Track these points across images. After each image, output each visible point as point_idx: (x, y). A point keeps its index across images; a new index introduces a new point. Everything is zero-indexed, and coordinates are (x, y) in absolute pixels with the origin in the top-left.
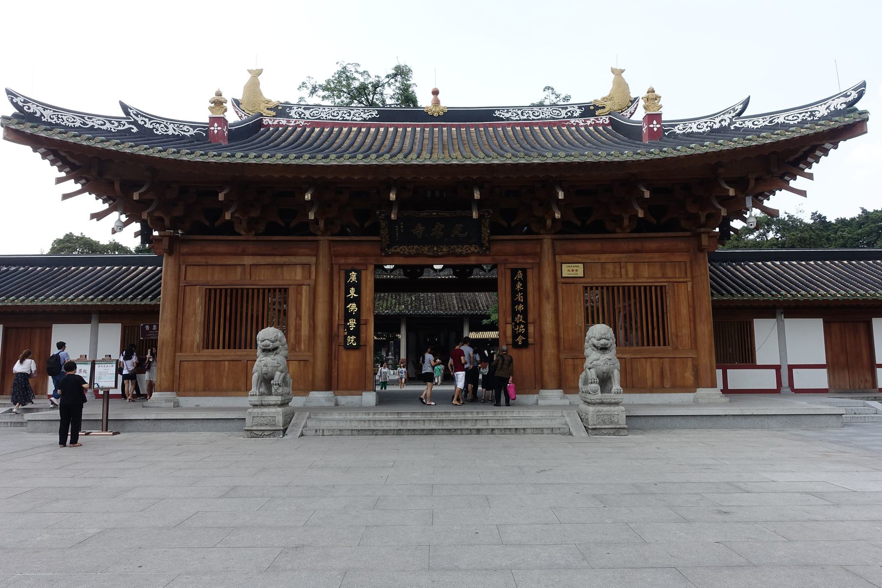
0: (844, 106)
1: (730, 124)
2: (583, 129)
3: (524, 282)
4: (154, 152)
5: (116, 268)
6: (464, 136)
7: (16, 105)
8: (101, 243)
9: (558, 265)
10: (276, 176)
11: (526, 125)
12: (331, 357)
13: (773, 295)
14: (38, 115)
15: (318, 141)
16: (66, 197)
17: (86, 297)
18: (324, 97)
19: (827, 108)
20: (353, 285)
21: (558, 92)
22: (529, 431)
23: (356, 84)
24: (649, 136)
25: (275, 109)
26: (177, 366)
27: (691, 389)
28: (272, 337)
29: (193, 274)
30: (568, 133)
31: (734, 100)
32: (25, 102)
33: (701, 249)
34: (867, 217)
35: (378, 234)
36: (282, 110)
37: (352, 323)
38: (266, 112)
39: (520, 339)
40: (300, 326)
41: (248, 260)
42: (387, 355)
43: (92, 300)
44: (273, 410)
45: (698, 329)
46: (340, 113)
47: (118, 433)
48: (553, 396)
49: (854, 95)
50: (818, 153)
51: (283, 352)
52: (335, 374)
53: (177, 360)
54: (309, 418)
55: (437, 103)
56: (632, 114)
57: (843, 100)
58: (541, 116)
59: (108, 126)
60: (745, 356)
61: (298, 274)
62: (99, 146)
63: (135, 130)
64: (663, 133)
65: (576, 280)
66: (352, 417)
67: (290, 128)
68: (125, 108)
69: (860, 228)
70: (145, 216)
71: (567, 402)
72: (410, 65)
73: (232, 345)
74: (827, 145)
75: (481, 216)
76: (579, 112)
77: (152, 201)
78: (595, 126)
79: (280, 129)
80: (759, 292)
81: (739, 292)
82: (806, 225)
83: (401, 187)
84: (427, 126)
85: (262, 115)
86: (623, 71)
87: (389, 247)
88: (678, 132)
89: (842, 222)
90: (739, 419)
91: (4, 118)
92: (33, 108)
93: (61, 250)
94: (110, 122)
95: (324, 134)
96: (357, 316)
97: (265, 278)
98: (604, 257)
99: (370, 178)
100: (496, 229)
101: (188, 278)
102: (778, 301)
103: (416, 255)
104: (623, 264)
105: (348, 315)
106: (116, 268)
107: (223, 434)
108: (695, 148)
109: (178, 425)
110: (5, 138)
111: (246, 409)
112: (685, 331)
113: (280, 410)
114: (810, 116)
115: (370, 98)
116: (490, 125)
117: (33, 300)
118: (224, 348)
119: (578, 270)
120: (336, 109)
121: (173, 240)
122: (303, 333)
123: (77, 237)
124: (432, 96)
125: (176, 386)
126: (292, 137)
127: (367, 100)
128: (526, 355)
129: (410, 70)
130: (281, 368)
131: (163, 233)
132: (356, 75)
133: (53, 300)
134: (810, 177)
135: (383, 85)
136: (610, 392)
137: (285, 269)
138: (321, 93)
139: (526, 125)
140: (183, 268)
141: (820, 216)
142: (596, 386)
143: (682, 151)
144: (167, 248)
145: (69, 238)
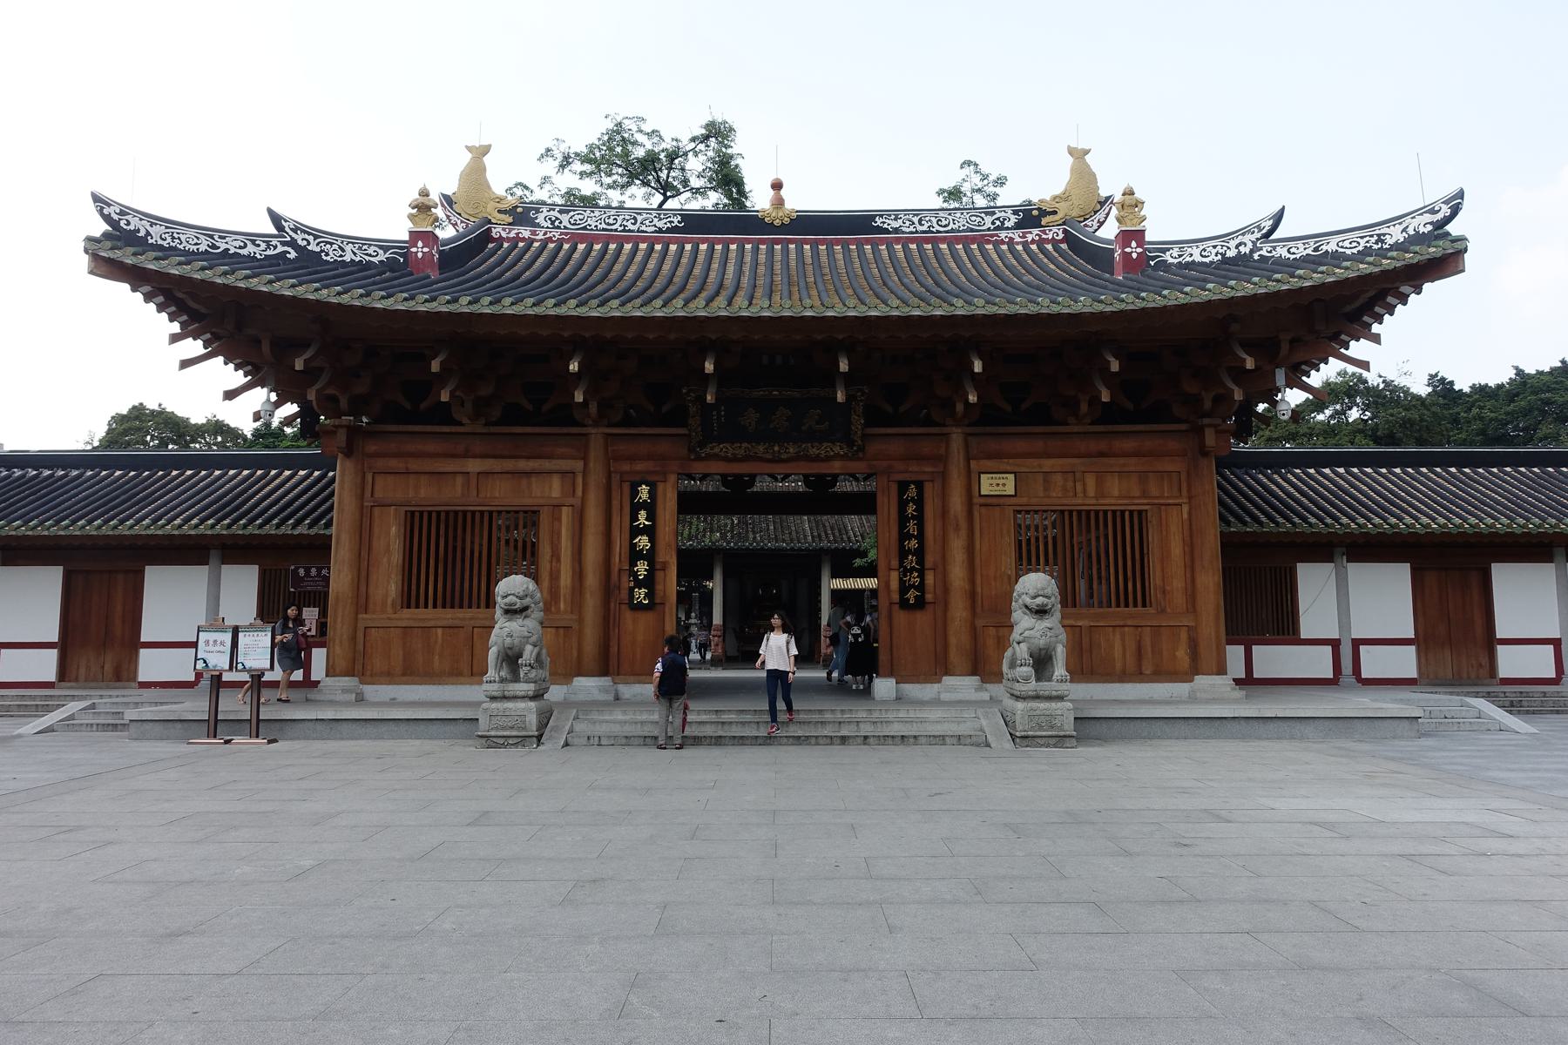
0: (1430, 228)
1: (1252, 251)
2: (1019, 248)
3: (920, 502)
4: (327, 295)
5: (246, 472)
6: (824, 259)
7: (107, 219)
8: (193, 421)
9: (974, 476)
10: (523, 333)
11: (927, 240)
12: (608, 622)
13: (1327, 525)
14: (142, 233)
15: (585, 268)
16: (185, 364)
17: (202, 521)
18: (582, 174)
19: (1404, 230)
20: (644, 505)
21: (985, 170)
22: (923, 740)
23: (639, 153)
24: (1124, 267)
25: (512, 211)
26: (360, 635)
27: (1187, 676)
28: (520, 590)
29: (385, 488)
30: (995, 256)
31: (1261, 212)
32: (122, 213)
33: (1204, 453)
34: (1524, 384)
35: (684, 425)
36: (522, 214)
37: (642, 568)
38: (496, 217)
39: (911, 595)
40: (559, 571)
41: (474, 466)
42: (688, 617)
43: (213, 526)
44: (521, 705)
45: (1198, 581)
46: (620, 219)
47: (275, 741)
48: (961, 686)
49: (1446, 210)
50: (1390, 299)
51: (537, 614)
52: (614, 650)
53: (361, 626)
54: (576, 718)
55: (779, 202)
56: (1101, 224)
57: (1428, 218)
60: (1282, 625)
61: (555, 489)
62: (241, 285)
63: (293, 255)
64: (1146, 263)
65: (1002, 501)
66: (644, 717)
67: (536, 244)
68: (276, 219)
69: (1512, 401)
70: (311, 396)
71: (985, 696)
72: (732, 120)
73: (466, 602)
74: (1405, 289)
75: (849, 398)
76: (1014, 219)
77: (321, 370)
78: (1041, 243)
79: (521, 244)
80: (1305, 520)
81: (1272, 519)
82: (1418, 398)
83: (721, 349)
84: (762, 242)
85: (490, 222)
86: (1087, 152)
87: (702, 445)
88: (1171, 260)
89: (1481, 391)
90: (1255, 723)
91: (89, 239)
92: (135, 223)
93: (126, 432)
94: (253, 242)
95: (593, 254)
96: (650, 557)
97: (501, 494)
98: (1048, 464)
99: (672, 336)
100: (875, 417)
101: (377, 495)
103: (746, 458)
104: (1078, 475)
105: (635, 555)
106: (246, 472)
107: (441, 742)
108: (1192, 294)
109: (370, 728)
110: (91, 272)
111: (479, 704)
112: (1178, 584)
113: (532, 704)
115: (663, 175)
116: (868, 241)
117: (115, 527)
118: (435, 606)
119: (1007, 485)
120: (613, 212)
121: (354, 432)
122: (562, 583)
123: (153, 411)
124: (772, 192)
125: (358, 667)
126: (541, 260)
127: (658, 180)
128: (922, 619)
129: (731, 129)
130: (534, 639)
131: (337, 422)
132: (640, 138)
133: (148, 527)
134: (1376, 339)
135: (686, 154)
136: (1050, 680)
137: (533, 479)
138: (578, 166)
139: (927, 240)
140: (369, 477)
141: (1443, 379)
142: (1027, 670)
143: (1173, 298)
144: (344, 445)
145: (138, 412)
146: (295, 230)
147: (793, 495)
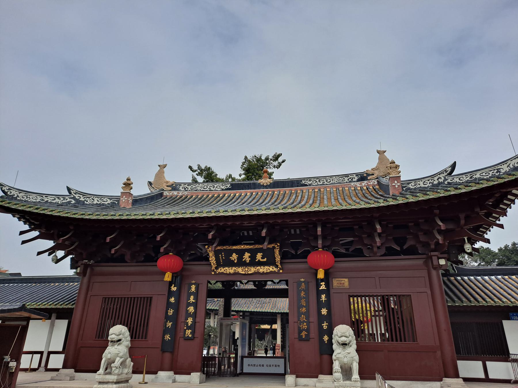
7: (3, 191)
14: (15, 196)
16: (24, 242)
20: (192, 293)
32: (9, 189)
36: (174, 187)
39: (304, 334)
46: (208, 187)
58: (332, 182)
59: (57, 200)
68: (69, 189)
76: (356, 178)
83: (271, 228)
85: (163, 190)
88: (412, 187)
92: (13, 192)
102: (500, 306)
114: (497, 172)
130: (121, 354)
146: (75, 194)
147: (252, 290)
